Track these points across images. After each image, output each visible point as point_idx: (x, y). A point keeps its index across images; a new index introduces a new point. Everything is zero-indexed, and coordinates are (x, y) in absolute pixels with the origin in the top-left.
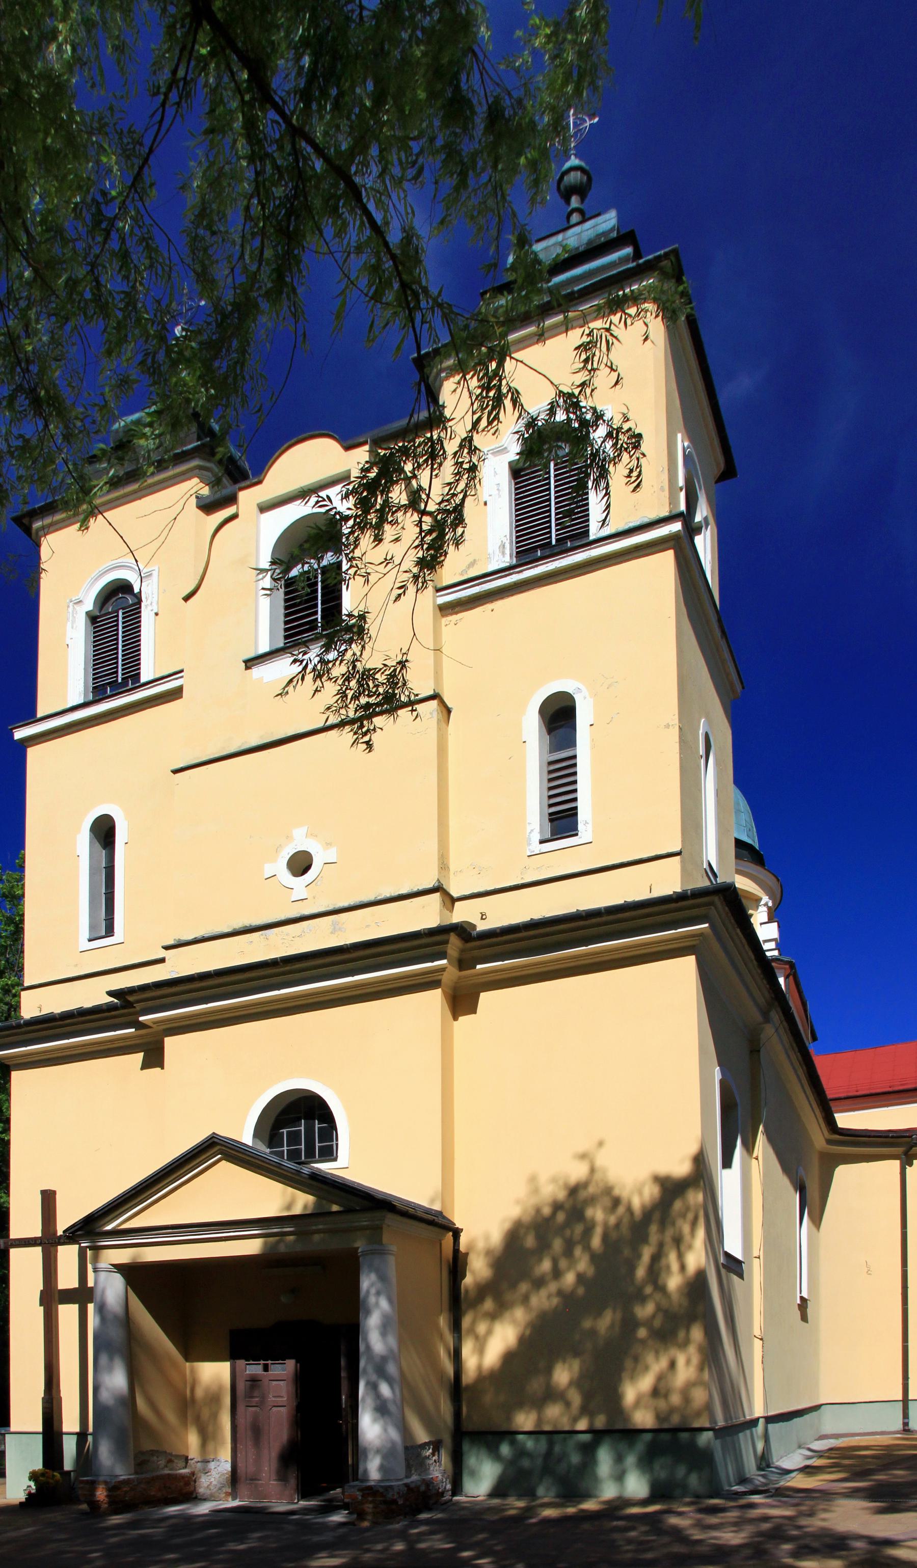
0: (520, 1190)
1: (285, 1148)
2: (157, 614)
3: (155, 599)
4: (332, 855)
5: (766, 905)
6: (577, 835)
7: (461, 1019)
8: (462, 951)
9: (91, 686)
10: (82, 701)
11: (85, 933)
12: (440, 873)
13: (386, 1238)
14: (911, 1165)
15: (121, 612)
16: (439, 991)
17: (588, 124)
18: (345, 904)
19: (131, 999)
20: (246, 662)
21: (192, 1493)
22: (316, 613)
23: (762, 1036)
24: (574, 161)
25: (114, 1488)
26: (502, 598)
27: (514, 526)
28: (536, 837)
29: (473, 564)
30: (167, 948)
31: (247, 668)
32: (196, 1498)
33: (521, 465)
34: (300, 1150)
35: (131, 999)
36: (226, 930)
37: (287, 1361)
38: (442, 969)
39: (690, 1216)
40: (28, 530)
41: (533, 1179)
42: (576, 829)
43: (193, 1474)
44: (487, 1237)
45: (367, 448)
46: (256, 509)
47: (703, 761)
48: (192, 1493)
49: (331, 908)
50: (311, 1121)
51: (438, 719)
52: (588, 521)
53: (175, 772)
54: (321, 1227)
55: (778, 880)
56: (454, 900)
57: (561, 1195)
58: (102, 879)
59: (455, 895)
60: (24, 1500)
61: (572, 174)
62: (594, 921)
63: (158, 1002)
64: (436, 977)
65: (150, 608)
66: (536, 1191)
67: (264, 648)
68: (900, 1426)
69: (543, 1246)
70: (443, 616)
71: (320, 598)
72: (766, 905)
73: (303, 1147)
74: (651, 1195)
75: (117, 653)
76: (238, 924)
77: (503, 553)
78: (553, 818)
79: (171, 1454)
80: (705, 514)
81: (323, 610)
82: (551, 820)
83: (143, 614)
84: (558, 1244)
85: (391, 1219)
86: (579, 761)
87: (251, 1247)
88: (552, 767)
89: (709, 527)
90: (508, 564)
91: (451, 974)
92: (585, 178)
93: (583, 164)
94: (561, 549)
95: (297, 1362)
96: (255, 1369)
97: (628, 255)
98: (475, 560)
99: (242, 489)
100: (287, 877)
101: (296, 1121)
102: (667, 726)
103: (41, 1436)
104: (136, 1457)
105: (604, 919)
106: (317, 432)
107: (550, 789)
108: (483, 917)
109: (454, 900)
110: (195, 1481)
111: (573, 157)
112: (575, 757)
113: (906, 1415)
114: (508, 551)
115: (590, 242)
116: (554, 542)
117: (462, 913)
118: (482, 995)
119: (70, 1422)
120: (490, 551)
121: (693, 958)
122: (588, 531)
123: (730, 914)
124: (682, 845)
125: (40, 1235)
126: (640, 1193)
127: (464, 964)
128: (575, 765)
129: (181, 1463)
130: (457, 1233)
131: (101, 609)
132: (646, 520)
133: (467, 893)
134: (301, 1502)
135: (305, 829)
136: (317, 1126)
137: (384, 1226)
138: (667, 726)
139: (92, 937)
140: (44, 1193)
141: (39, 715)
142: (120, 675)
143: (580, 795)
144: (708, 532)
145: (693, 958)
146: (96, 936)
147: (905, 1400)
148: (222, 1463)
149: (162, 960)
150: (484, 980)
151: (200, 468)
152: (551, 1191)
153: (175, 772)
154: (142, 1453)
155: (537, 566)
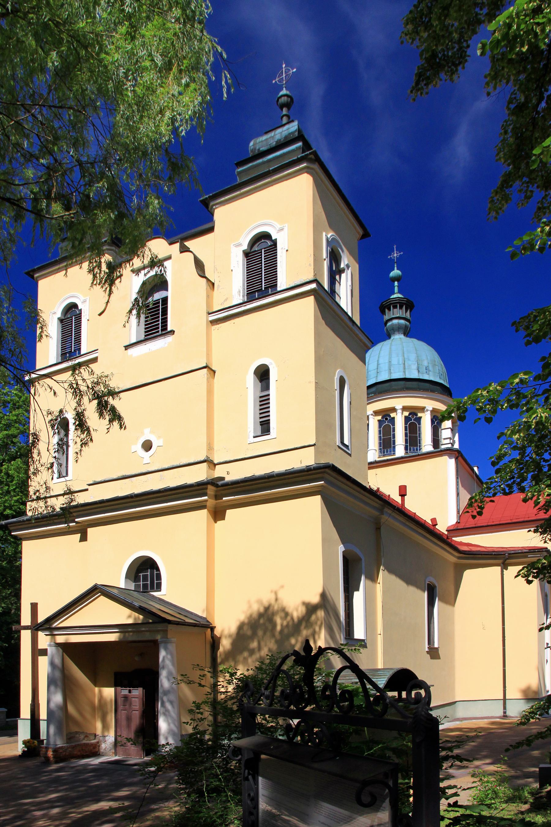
0: (245, 607)
7: (218, 522)
8: (216, 491)
9: (60, 353)
10: (55, 362)
12: (207, 452)
13: (169, 636)
14: (507, 569)
15: (74, 317)
16: (206, 510)
18: (166, 466)
19: (71, 511)
20: (125, 347)
21: (97, 752)
23: (382, 520)
24: (284, 92)
25: (55, 751)
28: (252, 435)
30: (89, 485)
31: (126, 349)
32: (99, 754)
33: (249, 250)
35: (71, 511)
36: (115, 477)
37: (139, 688)
38: (206, 501)
39: (319, 623)
40: (32, 277)
41: (249, 602)
43: (98, 742)
44: (229, 629)
47: (337, 393)
48: (97, 752)
49: (160, 468)
56: (215, 465)
57: (262, 610)
59: (216, 462)
60: (21, 754)
61: (283, 98)
62: (310, 472)
64: (204, 504)
65: (85, 317)
66: (250, 607)
67: (134, 340)
68: (501, 714)
69: (254, 634)
73: (149, 582)
74: (302, 611)
76: (120, 474)
77: (240, 295)
78: (262, 423)
79: (87, 733)
81: (162, 308)
82: (261, 425)
84: (260, 633)
85: (170, 627)
86: (271, 397)
87: (112, 637)
91: (211, 502)
93: (288, 93)
95: (143, 689)
96: (125, 692)
97: (300, 146)
100: (142, 452)
101: (146, 570)
102: (310, 382)
103: (30, 721)
104: (67, 735)
107: (260, 409)
109: (215, 465)
110: (99, 746)
112: (269, 395)
113: (505, 708)
114: (241, 294)
115: (286, 137)
116: (263, 289)
117: (219, 472)
118: (227, 511)
119: (43, 714)
122: (277, 285)
125: (30, 624)
126: (297, 610)
127: (217, 497)
128: (269, 399)
129: (92, 737)
130: (212, 629)
131: (65, 316)
134: (145, 758)
137: (169, 630)
138: (310, 382)
140: (32, 604)
141: (37, 368)
144: (349, 272)
147: (505, 699)
148: (111, 737)
149: (87, 490)
152: (256, 608)
154: (71, 733)
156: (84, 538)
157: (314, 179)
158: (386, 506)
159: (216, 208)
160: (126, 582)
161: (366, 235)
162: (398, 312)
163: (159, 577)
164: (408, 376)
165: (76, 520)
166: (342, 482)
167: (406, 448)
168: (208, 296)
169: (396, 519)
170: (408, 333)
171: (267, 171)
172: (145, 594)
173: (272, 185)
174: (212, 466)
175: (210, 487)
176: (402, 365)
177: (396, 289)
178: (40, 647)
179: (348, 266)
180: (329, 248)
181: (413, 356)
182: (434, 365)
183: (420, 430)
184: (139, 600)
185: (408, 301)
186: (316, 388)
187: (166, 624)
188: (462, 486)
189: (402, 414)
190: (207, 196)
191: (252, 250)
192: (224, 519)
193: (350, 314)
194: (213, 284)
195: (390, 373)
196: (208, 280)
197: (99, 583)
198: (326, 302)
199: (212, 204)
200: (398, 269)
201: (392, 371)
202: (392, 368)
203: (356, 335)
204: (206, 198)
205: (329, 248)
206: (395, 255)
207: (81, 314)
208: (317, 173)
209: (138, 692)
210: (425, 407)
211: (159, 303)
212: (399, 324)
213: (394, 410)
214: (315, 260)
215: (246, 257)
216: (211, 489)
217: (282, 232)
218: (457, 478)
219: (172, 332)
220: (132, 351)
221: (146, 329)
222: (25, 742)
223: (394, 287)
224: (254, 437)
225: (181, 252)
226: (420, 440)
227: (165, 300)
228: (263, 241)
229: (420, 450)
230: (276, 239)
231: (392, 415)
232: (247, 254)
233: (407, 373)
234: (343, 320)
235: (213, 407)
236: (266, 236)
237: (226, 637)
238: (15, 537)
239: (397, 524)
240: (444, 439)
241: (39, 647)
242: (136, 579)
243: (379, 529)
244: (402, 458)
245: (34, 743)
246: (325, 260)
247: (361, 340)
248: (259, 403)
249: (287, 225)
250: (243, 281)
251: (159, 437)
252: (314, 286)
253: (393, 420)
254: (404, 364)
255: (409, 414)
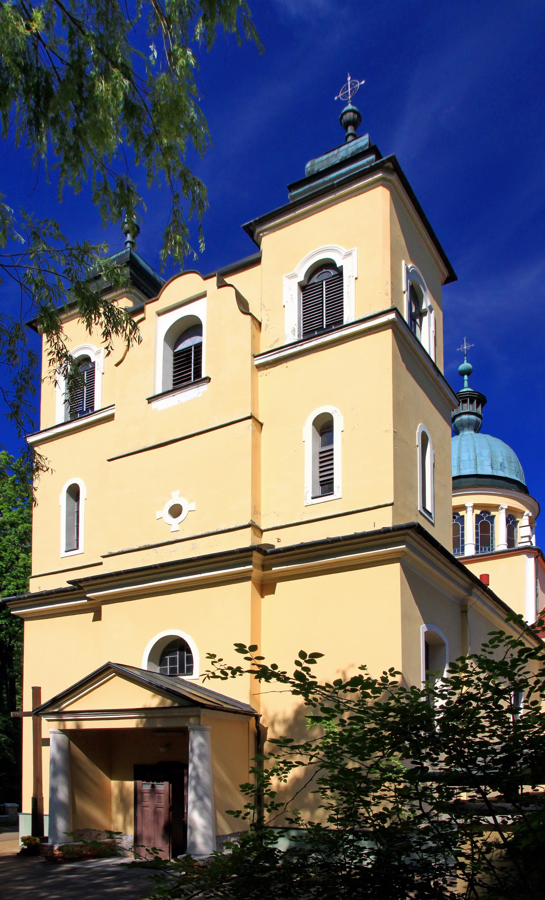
1: (168, 667)
2: (103, 374)
3: (103, 365)
4: (193, 506)
5: (528, 515)
6: (333, 494)
8: (263, 560)
10: (63, 422)
11: (63, 547)
12: (252, 516)
16: (250, 582)
17: (358, 85)
18: (200, 533)
19: (81, 585)
20: (148, 399)
22: (191, 371)
24: (350, 107)
26: (292, 360)
27: (302, 318)
28: (310, 495)
29: (277, 341)
30: (104, 557)
31: (149, 403)
33: (306, 283)
34: (176, 668)
35: (81, 585)
36: (136, 547)
38: (251, 571)
42: (333, 491)
44: (284, 713)
45: (215, 279)
46: (155, 315)
47: (419, 450)
49: (192, 536)
50: (182, 652)
51: (253, 430)
52: (343, 314)
53: (109, 460)
54: (159, 715)
55: (536, 501)
56: (262, 531)
58: (74, 519)
59: (263, 528)
62: (387, 534)
63: (98, 586)
65: (99, 370)
67: (159, 391)
70: (259, 371)
71: (193, 362)
72: (528, 515)
73: (178, 666)
75: (83, 395)
77: (294, 334)
78: (322, 484)
80: (429, 304)
81: (194, 369)
82: (321, 485)
83: (96, 374)
85: (203, 711)
87: (131, 724)
88: (322, 455)
89: (433, 311)
90: (296, 340)
91: (257, 573)
92: (356, 116)
93: (355, 108)
94: (329, 330)
95: (170, 783)
97: (373, 160)
98: (278, 339)
99: (147, 304)
100: (168, 518)
102: (386, 431)
103: (31, 816)
105: (343, 543)
106: (188, 271)
107: (321, 467)
108: (279, 540)
109: (262, 531)
111: (350, 104)
112: (332, 450)
114: (296, 333)
115: (353, 153)
116: (325, 327)
117: (267, 539)
118: (278, 584)
120: (286, 333)
121: (399, 564)
123: (423, 539)
124: (394, 499)
127: (265, 567)
128: (332, 454)
130: (257, 717)
132: (376, 312)
133: (270, 527)
135: (178, 492)
136: (185, 655)
138: (386, 431)
139: (68, 550)
140: (34, 688)
141: (41, 429)
142: (85, 407)
143: (335, 471)
144: (432, 315)
145: (399, 564)
146: (70, 549)
149: (101, 564)
150: (276, 576)
151: (127, 292)
153: (109, 460)
155: (311, 341)
156: (98, 617)
157: (391, 193)
158: (476, 585)
159: (264, 236)
160: (148, 664)
161: (451, 278)
162: (467, 407)
163: (190, 660)
164: (480, 472)
165: (88, 595)
166: (427, 550)
167: (477, 548)
168: (253, 337)
169: (485, 604)
170: (479, 430)
171: (331, 186)
172: (172, 678)
173: (337, 204)
174: (258, 533)
175: (255, 554)
176: (473, 462)
177: (466, 384)
178: (44, 736)
179: (431, 309)
180: (409, 281)
181: (486, 452)
182: (510, 462)
183: (492, 529)
184: (166, 682)
185: (480, 395)
186: (394, 438)
187: (199, 709)
188: (541, 589)
189: (473, 512)
190: (252, 221)
191: (310, 283)
192: (273, 593)
193: (434, 360)
194: (260, 324)
195: (460, 469)
196: (254, 318)
197: (114, 661)
198: (405, 339)
199: (258, 230)
200: (468, 362)
201: (461, 467)
202: (461, 465)
203: (441, 388)
204: (251, 224)
205: (409, 281)
206: (465, 347)
207: (94, 367)
208: (395, 187)
209: (163, 787)
210: (499, 505)
211: (191, 350)
212: (469, 419)
213: (463, 507)
214: (392, 289)
215: (303, 291)
216: (257, 557)
217: (349, 258)
218: (536, 578)
219: (208, 379)
220: (157, 405)
221: (174, 380)
222: (24, 839)
223: (464, 381)
224: (313, 498)
225: (219, 287)
226: (492, 540)
227: (198, 347)
228: (324, 271)
229: (492, 550)
230: (342, 267)
231: (461, 513)
232: (303, 287)
233: (478, 469)
234: (425, 367)
235: (259, 466)
236: (329, 264)
237: (279, 723)
238: (15, 616)
239: (485, 608)
240: (519, 543)
241: (43, 737)
242: (162, 662)
243: (466, 612)
244: (473, 557)
245: (35, 840)
246: (404, 292)
247: (446, 396)
248: (318, 460)
249: (356, 249)
250: (299, 318)
251: (191, 501)
252: (392, 316)
253: (462, 519)
254: (476, 460)
255: (481, 513)
